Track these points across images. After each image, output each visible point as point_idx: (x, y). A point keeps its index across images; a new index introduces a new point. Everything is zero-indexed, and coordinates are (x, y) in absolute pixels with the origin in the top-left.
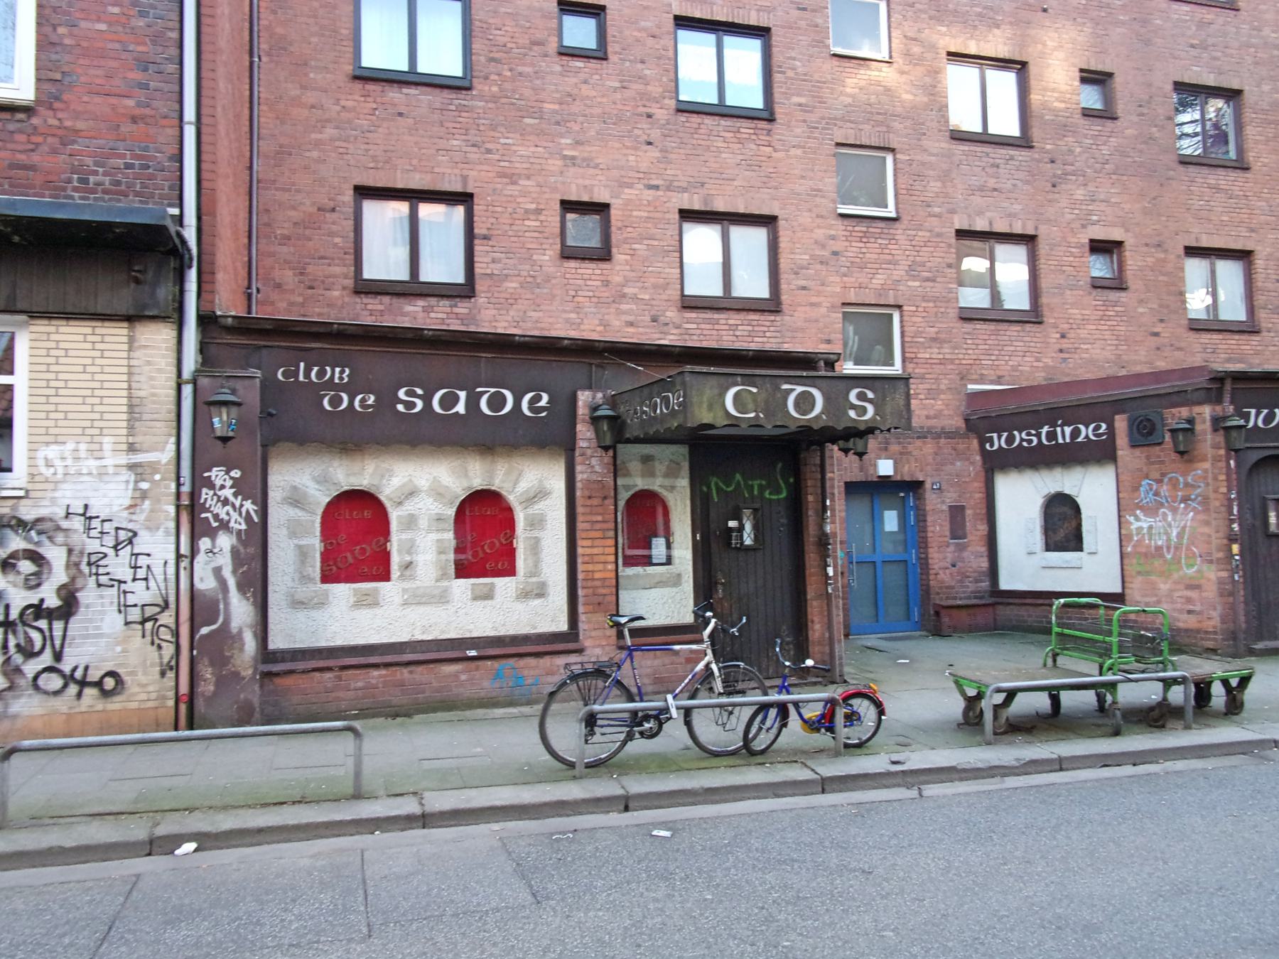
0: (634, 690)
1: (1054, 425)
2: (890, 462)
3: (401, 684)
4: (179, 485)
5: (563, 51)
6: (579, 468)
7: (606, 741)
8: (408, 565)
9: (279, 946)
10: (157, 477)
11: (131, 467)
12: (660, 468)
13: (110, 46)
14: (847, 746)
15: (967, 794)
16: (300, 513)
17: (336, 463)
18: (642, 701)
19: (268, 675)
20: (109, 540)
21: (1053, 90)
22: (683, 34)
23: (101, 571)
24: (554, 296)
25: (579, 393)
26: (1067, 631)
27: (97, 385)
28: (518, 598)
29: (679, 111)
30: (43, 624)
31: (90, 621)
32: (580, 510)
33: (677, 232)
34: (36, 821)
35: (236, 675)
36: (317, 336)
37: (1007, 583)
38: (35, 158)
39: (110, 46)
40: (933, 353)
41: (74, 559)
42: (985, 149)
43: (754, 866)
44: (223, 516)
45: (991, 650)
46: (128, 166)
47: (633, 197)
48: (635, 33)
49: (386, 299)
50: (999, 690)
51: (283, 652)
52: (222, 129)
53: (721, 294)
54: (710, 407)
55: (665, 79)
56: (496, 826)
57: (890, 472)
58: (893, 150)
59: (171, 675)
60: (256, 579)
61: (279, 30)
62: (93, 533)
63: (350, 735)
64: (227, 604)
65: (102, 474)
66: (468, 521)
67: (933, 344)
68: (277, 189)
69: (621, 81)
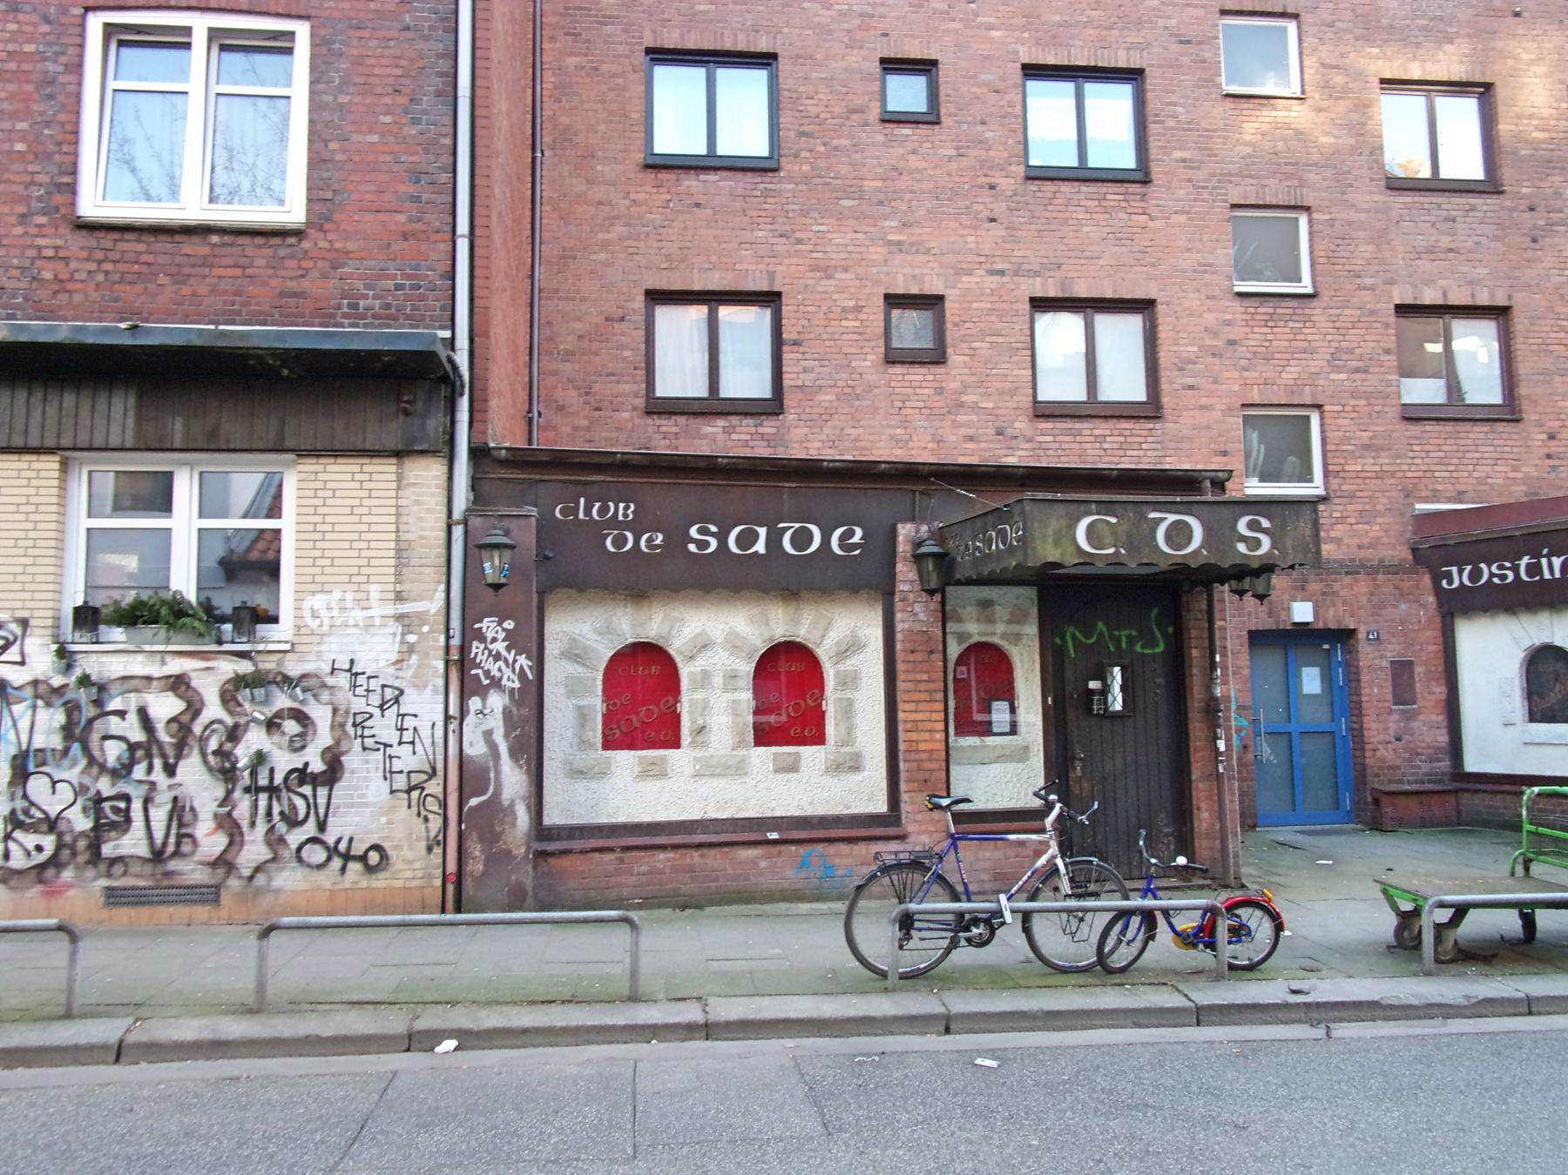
0: (960, 888)
1: (1538, 556)
2: (1308, 606)
3: (691, 869)
4: (448, 638)
5: (887, 117)
6: (899, 616)
7: (925, 948)
8: (701, 730)
9: (536, 1160)
10: (426, 629)
11: (399, 618)
12: (1000, 612)
13: (382, 158)
14: (1232, 967)
15: (1392, 1038)
16: (580, 669)
17: (620, 612)
18: (969, 900)
19: (542, 855)
20: (375, 699)
21: (1531, 117)
22: (1033, 86)
23: (367, 732)
24: (876, 409)
25: (899, 526)
26: (1542, 830)
27: (365, 527)
28: (827, 771)
29: (1028, 178)
30: (307, 790)
31: (355, 788)
32: (900, 666)
33: (1028, 325)
34: (294, 1006)
35: (508, 853)
36: (599, 468)
37: (1474, 763)
38: (306, 284)
39: (382, 158)
40: (1368, 464)
41: (339, 719)
42: (1435, 200)
43: (1096, 1110)
44: (495, 672)
45: (1450, 851)
46: (398, 287)
47: (973, 286)
48: (974, 90)
49: (682, 420)
50: (1442, 905)
51: (560, 828)
52: (497, 239)
53: (1084, 398)
54: (1057, 543)
55: (1011, 141)
56: (789, 1043)
57: (1309, 618)
58: (1307, 209)
59: (438, 850)
60: (530, 744)
61: (564, 120)
62: (359, 691)
63: (626, 927)
64: (498, 773)
65: (368, 626)
66: (783, 679)
67: (1366, 453)
68: (560, 299)
69: (957, 148)
